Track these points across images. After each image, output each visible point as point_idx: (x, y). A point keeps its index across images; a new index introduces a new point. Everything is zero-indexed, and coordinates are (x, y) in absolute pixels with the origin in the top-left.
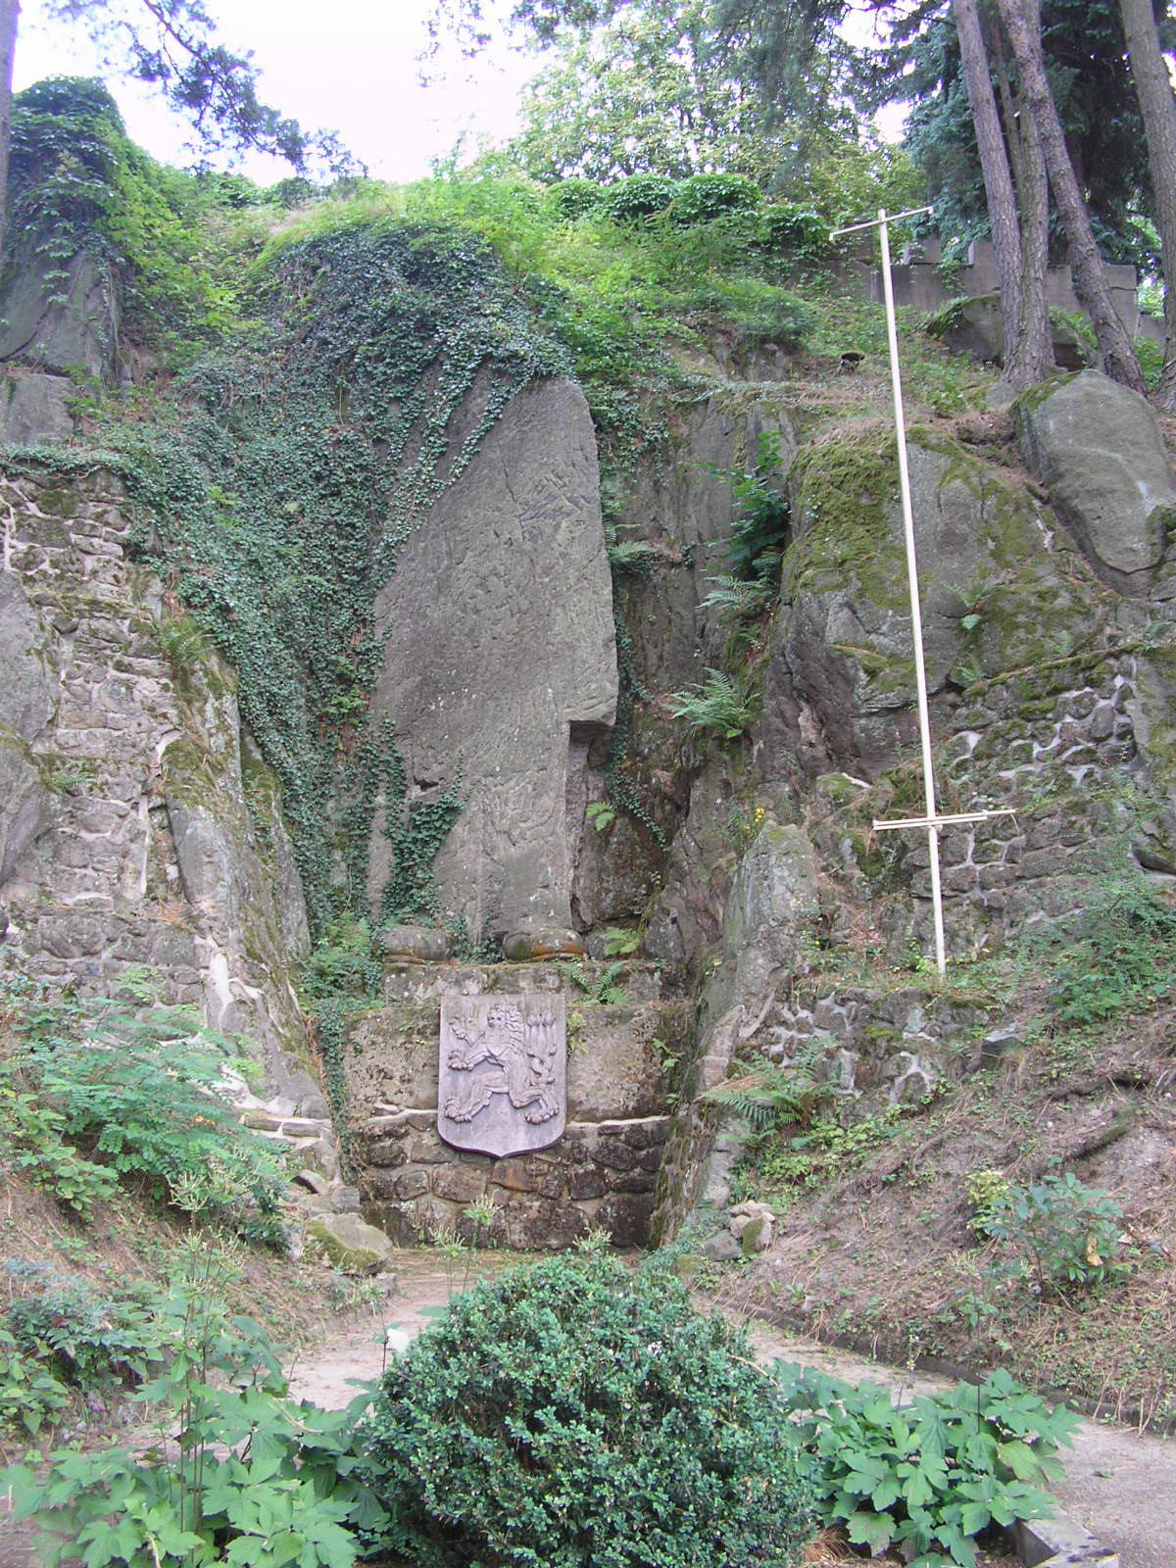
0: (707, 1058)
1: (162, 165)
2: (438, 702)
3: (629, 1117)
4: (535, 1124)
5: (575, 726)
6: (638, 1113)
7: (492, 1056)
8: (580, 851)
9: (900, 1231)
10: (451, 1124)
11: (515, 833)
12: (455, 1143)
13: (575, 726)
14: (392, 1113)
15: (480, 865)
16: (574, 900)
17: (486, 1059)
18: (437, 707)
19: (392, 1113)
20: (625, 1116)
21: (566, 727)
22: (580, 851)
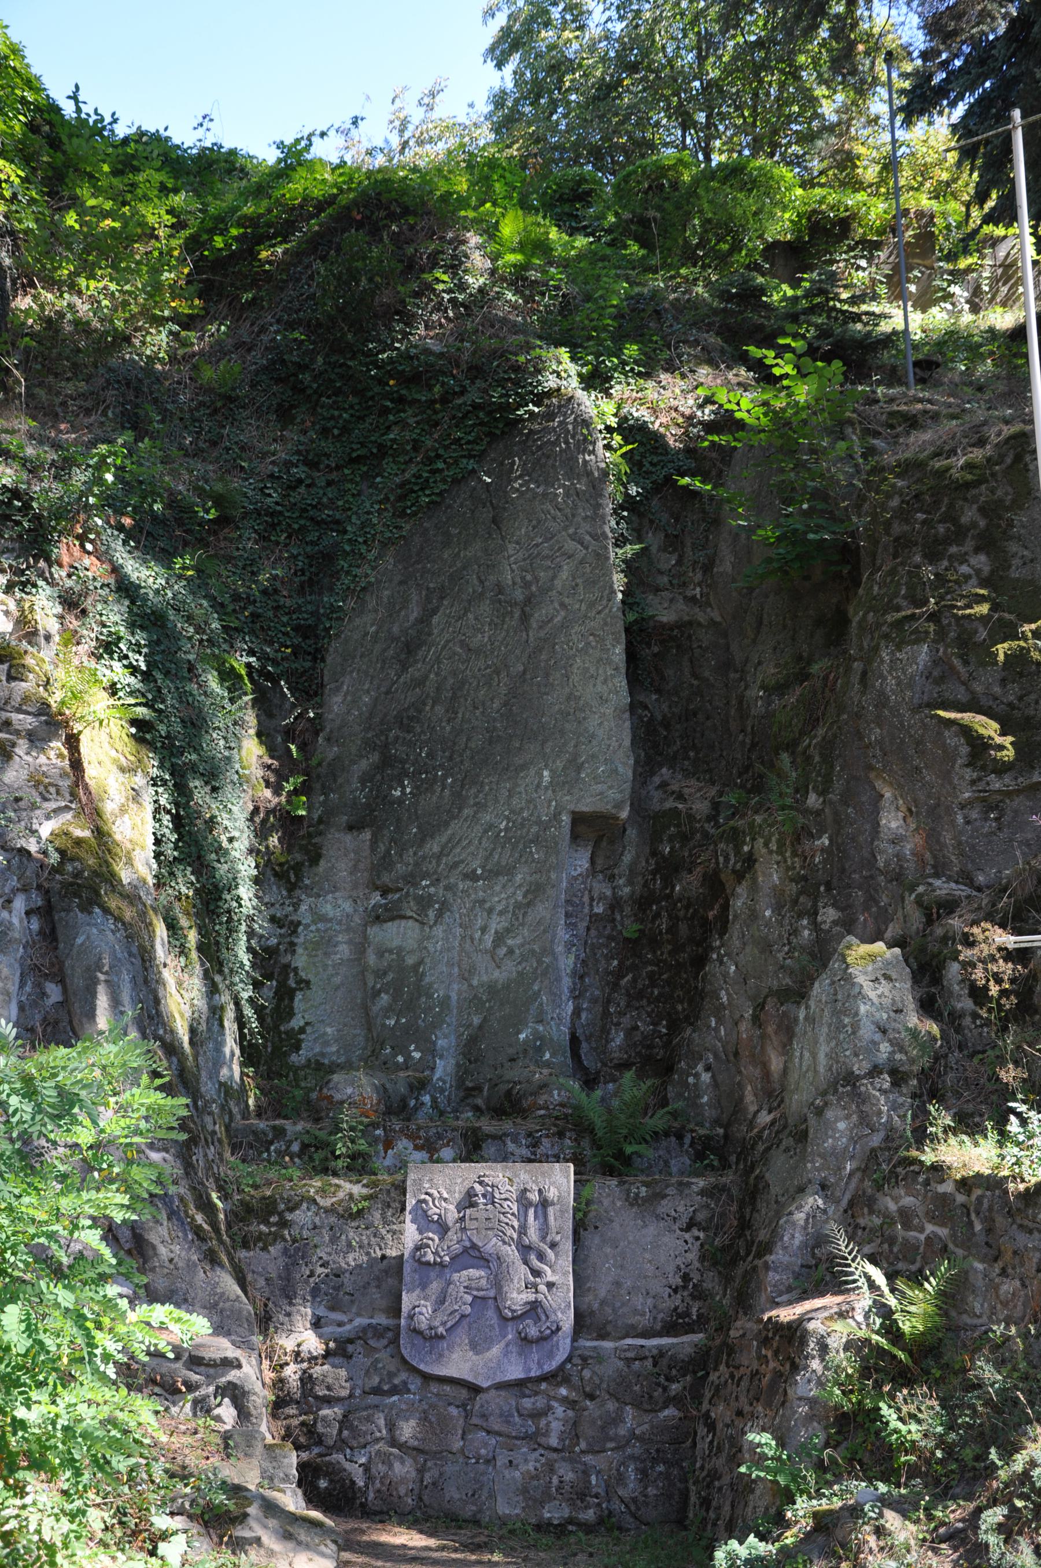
0: (770, 1258)
1: (505, 78)
2: (404, 788)
3: (659, 1334)
4: (532, 1342)
5: (579, 820)
6: (670, 1328)
7: (474, 1246)
8: (581, 977)
9: (35, 1447)
10: (418, 1341)
11: (55, 970)
12: (422, 1367)
13: (579, 820)
14: (340, 1324)
15: (455, 991)
16: (574, 1040)
17: (465, 1250)
18: (403, 792)
19: (340, 1324)
20: (646, 1334)
21: (565, 818)
22: (581, 977)
